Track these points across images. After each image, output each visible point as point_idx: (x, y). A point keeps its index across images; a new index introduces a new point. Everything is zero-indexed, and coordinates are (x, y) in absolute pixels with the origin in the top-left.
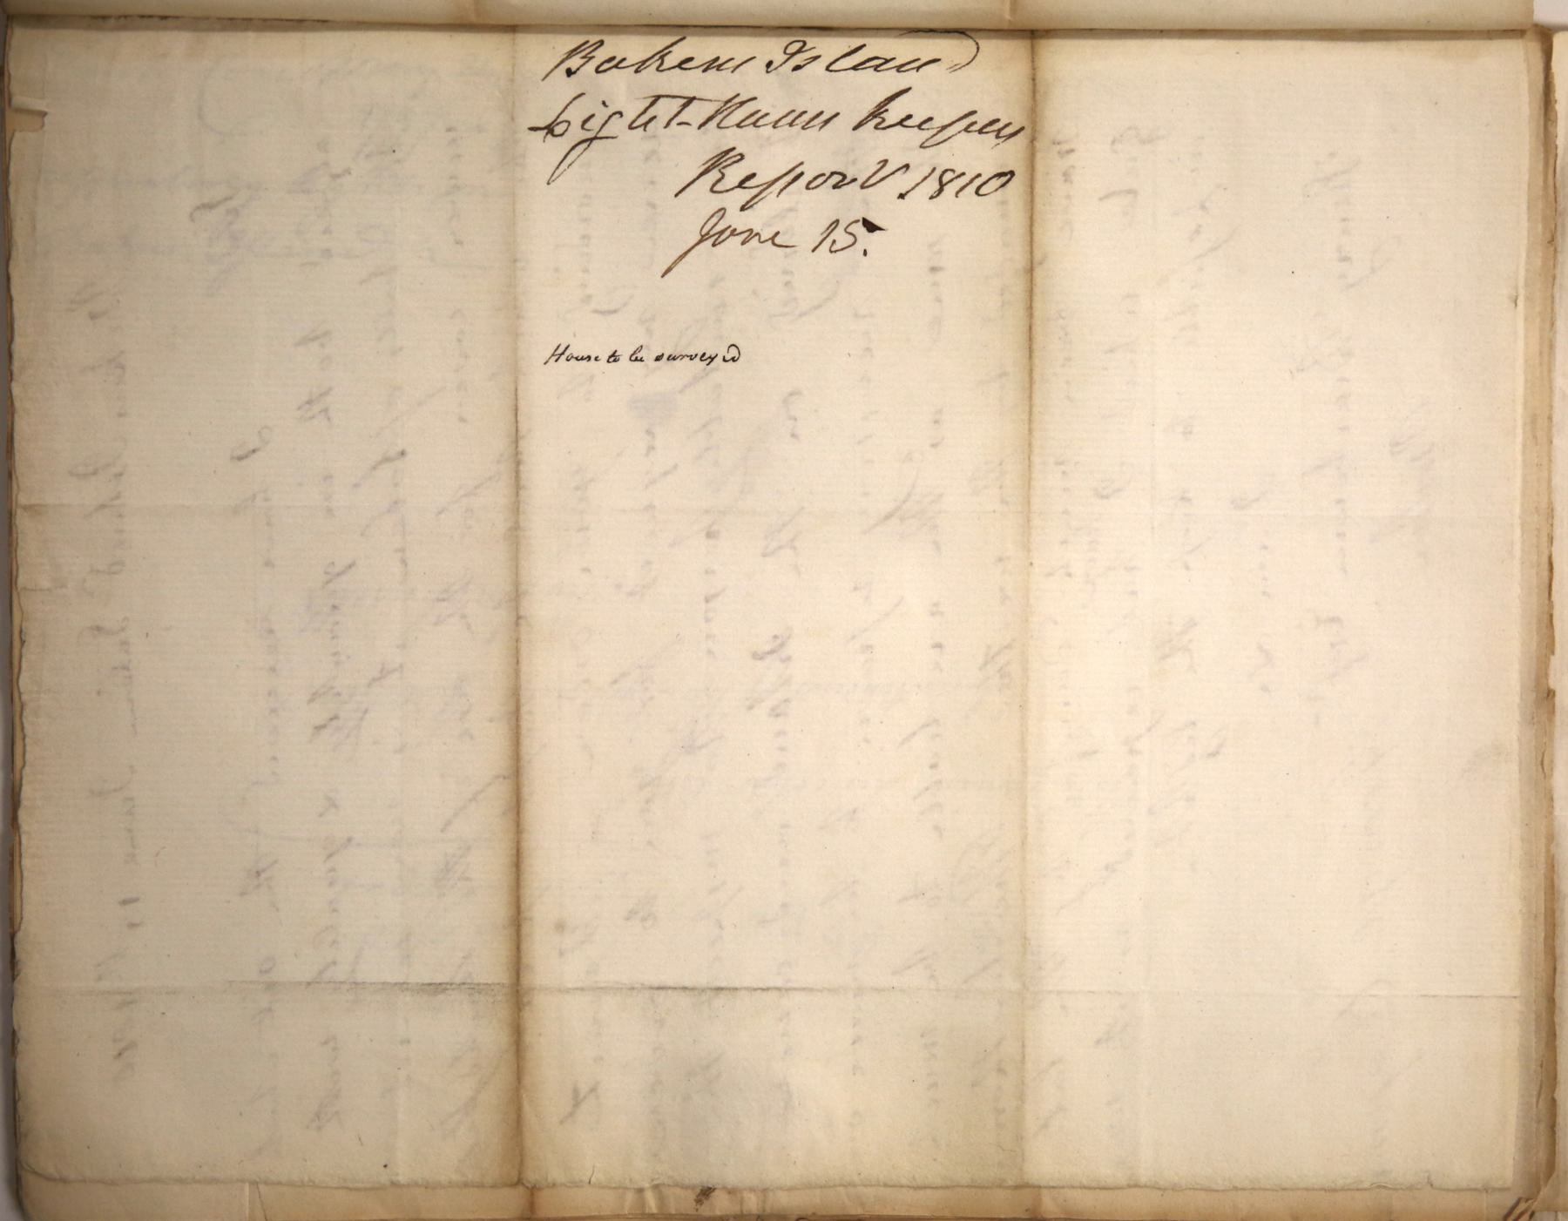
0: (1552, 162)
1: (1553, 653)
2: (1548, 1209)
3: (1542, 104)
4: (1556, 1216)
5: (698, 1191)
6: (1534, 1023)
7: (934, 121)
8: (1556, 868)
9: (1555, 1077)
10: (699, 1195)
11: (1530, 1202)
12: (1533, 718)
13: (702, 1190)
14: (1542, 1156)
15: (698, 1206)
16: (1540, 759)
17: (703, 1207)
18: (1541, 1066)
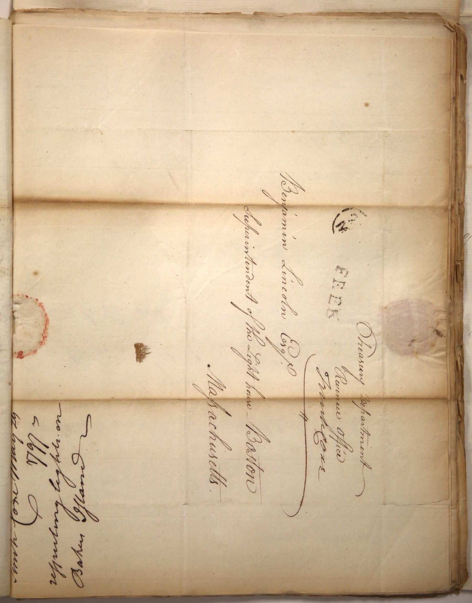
0: (53, 10)
1: (240, 13)
2: (458, 19)
3: (30, 14)
4: (462, 17)
5: (438, 336)
6: (378, 20)
7: (15, 462)
8: (321, 12)
9: (401, 13)
10: (439, 336)
11: (445, 22)
12: (262, 20)
13: (437, 335)
14: (429, 18)
15: (443, 336)
16: (279, 17)
17: (443, 334)
18: (395, 17)
